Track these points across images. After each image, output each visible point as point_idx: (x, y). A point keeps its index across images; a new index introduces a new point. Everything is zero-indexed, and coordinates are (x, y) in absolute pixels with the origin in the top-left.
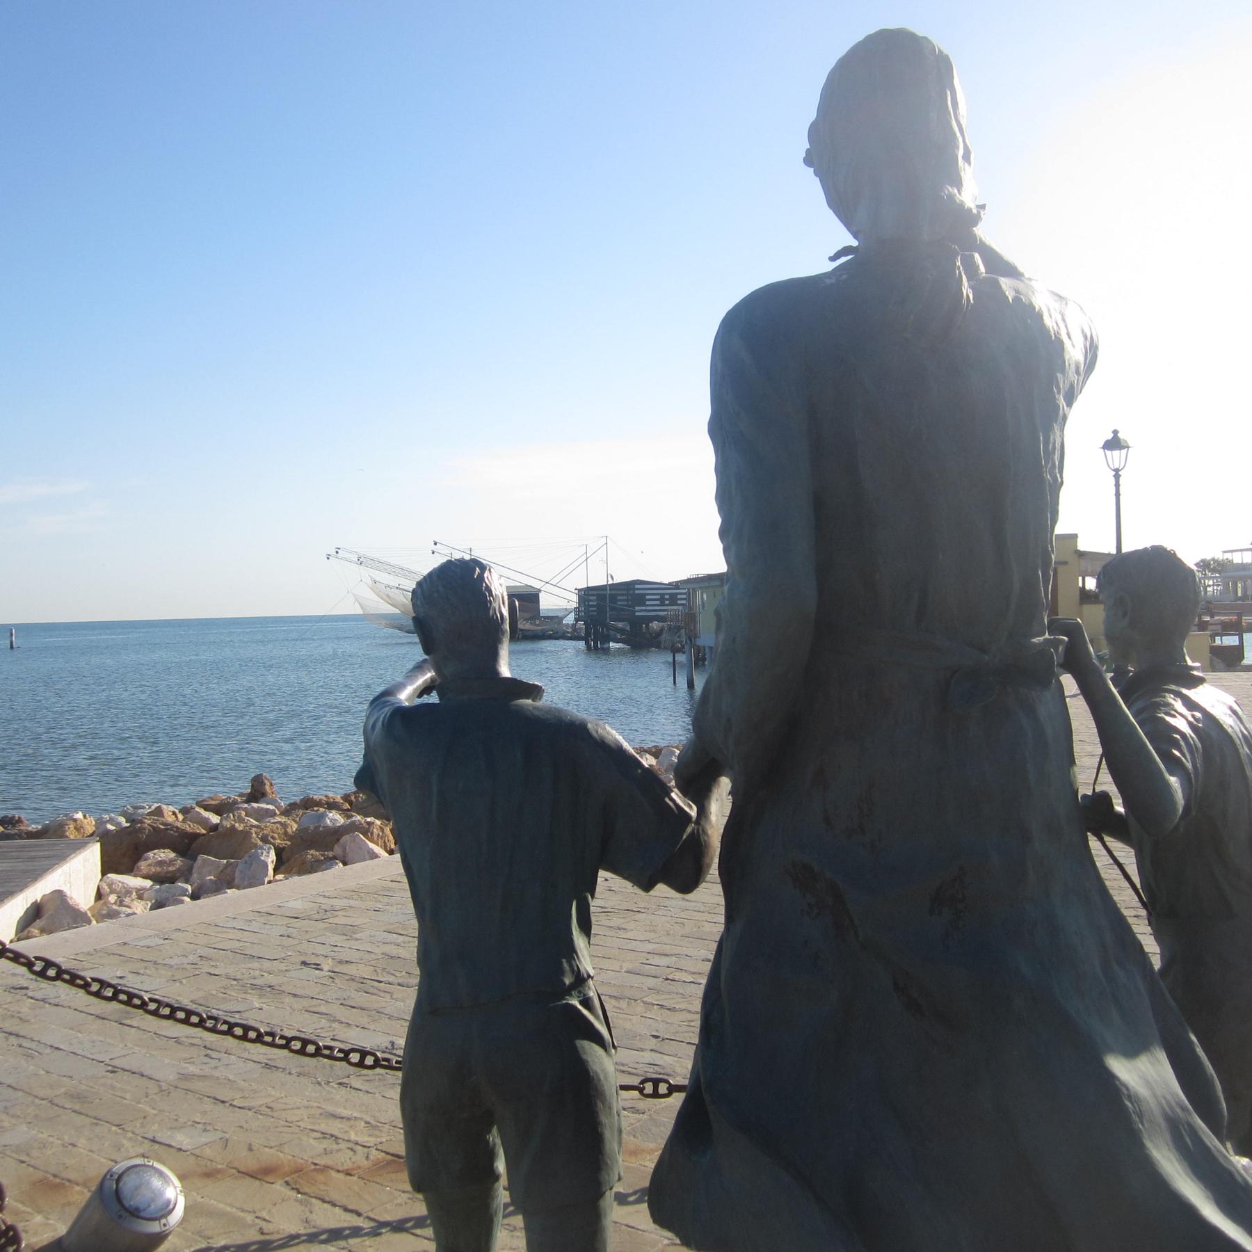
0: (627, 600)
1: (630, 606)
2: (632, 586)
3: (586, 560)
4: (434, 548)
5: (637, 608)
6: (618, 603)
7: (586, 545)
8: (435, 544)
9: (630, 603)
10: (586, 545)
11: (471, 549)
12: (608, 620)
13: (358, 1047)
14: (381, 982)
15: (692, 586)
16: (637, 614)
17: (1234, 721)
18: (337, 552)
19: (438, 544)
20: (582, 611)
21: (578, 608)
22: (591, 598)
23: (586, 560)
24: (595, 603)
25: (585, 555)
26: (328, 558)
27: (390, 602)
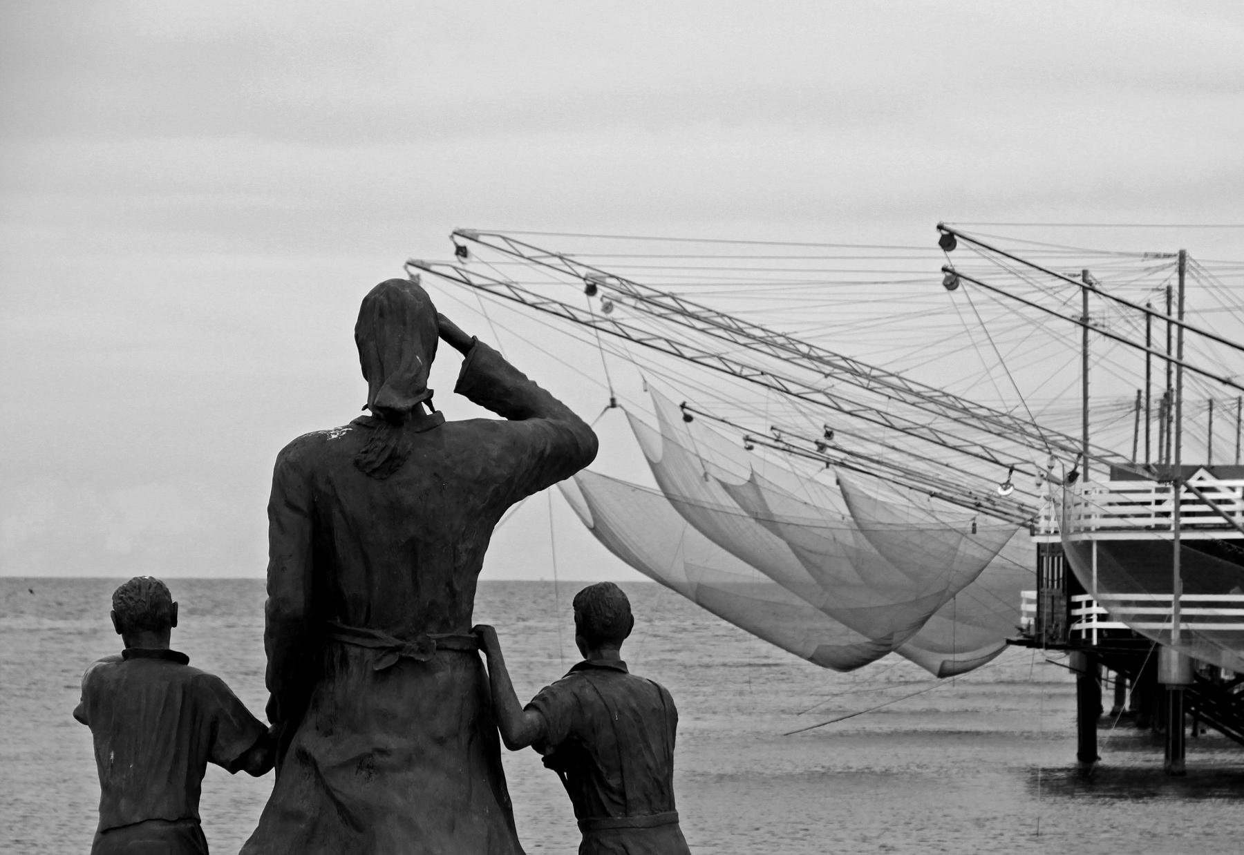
8: (948, 241)
11: (1182, 256)
18: (462, 251)
19: (964, 285)
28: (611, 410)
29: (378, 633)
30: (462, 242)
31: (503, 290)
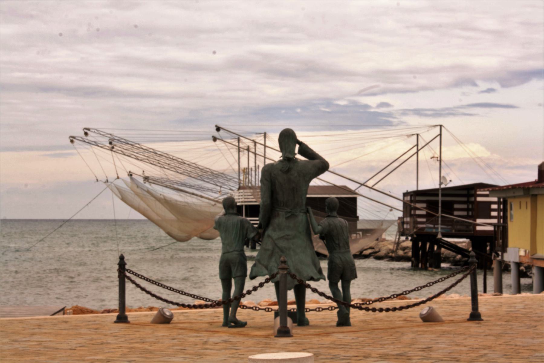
0: (467, 210)
1: (467, 217)
2: (473, 192)
3: (417, 153)
4: (216, 134)
5: (479, 221)
6: (456, 213)
7: (418, 135)
8: (218, 129)
9: (470, 213)
10: (418, 135)
12: (439, 236)
13: (177, 103)
14: (97, 349)
15: (504, 195)
16: (478, 228)
17: (197, 199)
18: (86, 134)
19: (221, 131)
20: (407, 223)
21: (403, 218)
22: (418, 205)
23: (417, 153)
24: (423, 212)
25: (416, 148)
26: (72, 141)
27: (27, 321)
28: (117, 180)
29: (286, 208)
30: (86, 131)
31: (93, 143)
